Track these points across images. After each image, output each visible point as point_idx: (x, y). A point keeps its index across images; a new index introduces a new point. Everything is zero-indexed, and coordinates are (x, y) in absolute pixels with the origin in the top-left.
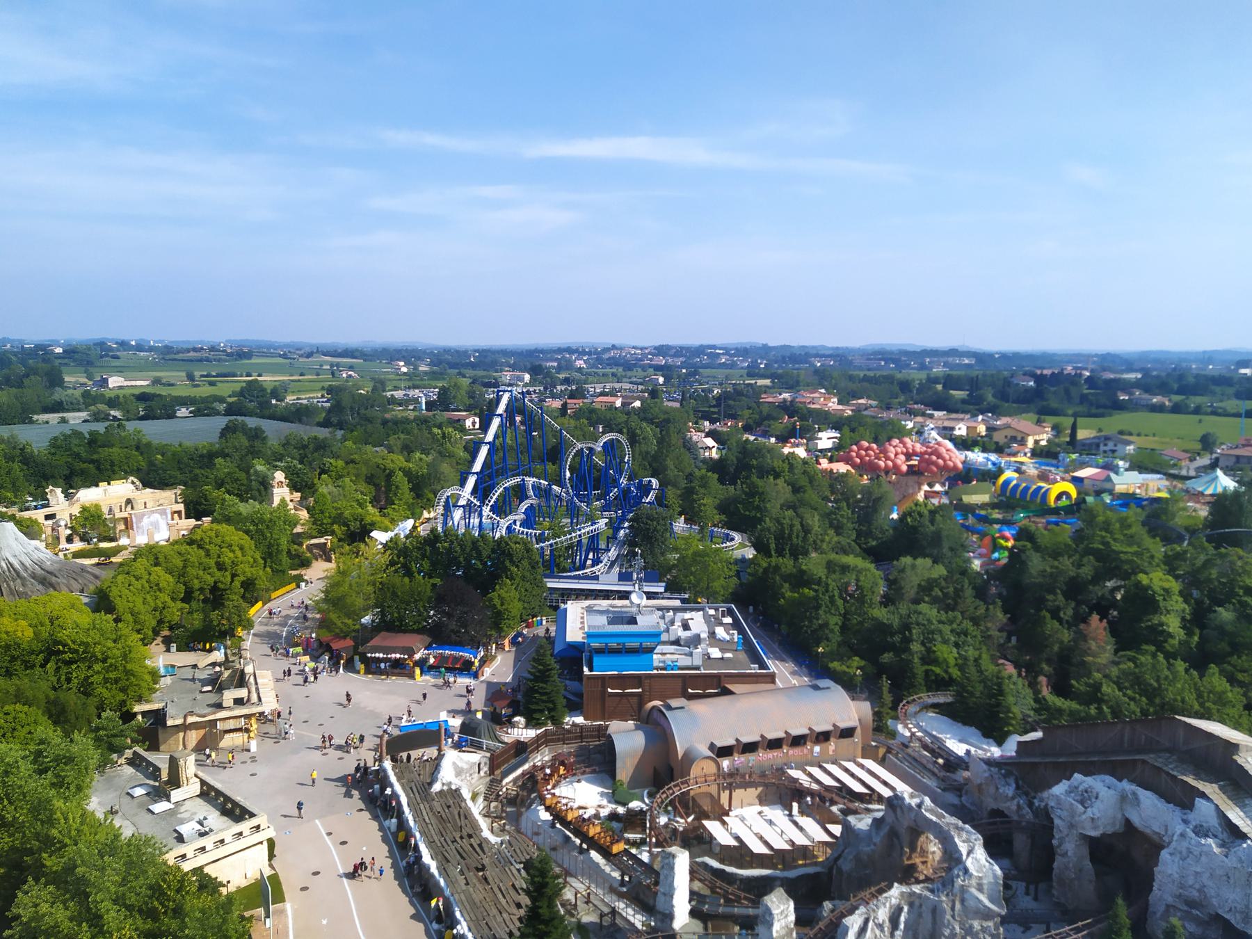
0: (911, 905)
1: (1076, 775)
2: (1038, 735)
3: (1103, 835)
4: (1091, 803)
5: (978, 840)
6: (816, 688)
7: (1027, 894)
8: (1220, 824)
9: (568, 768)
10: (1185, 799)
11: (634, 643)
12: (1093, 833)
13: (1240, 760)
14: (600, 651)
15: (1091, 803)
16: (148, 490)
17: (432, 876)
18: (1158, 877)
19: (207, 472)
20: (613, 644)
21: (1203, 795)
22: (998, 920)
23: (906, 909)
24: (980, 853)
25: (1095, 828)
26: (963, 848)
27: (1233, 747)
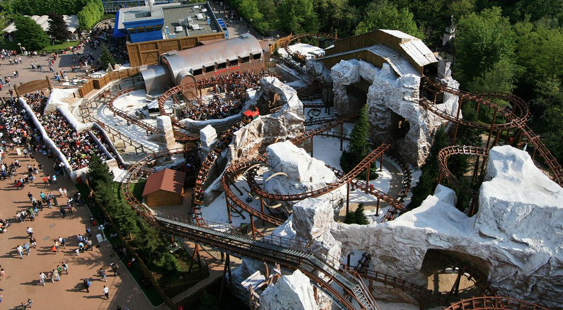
0: (266, 122)
1: (342, 60)
2: (333, 46)
3: (351, 84)
4: (345, 70)
5: (295, 93)
6: (242, 38)
7: (326, 112)
8: (391, 72)
9: (119, 90)
10: (378, 63)
11: (149, 26)
12: (348, 84)
13: (401, 45)
14: (133, 32)
15: (345, 70)
16: (527, 153)
17: (54, 148)
18: (368, 97)
19: (496, 274)
20: (141, 27)
21: (386, 62)
22: (302, 123)
23: (264, 124)
24: (296, 98)
25: (348, 81)
26: (288, 96)
27: (399, 40)
